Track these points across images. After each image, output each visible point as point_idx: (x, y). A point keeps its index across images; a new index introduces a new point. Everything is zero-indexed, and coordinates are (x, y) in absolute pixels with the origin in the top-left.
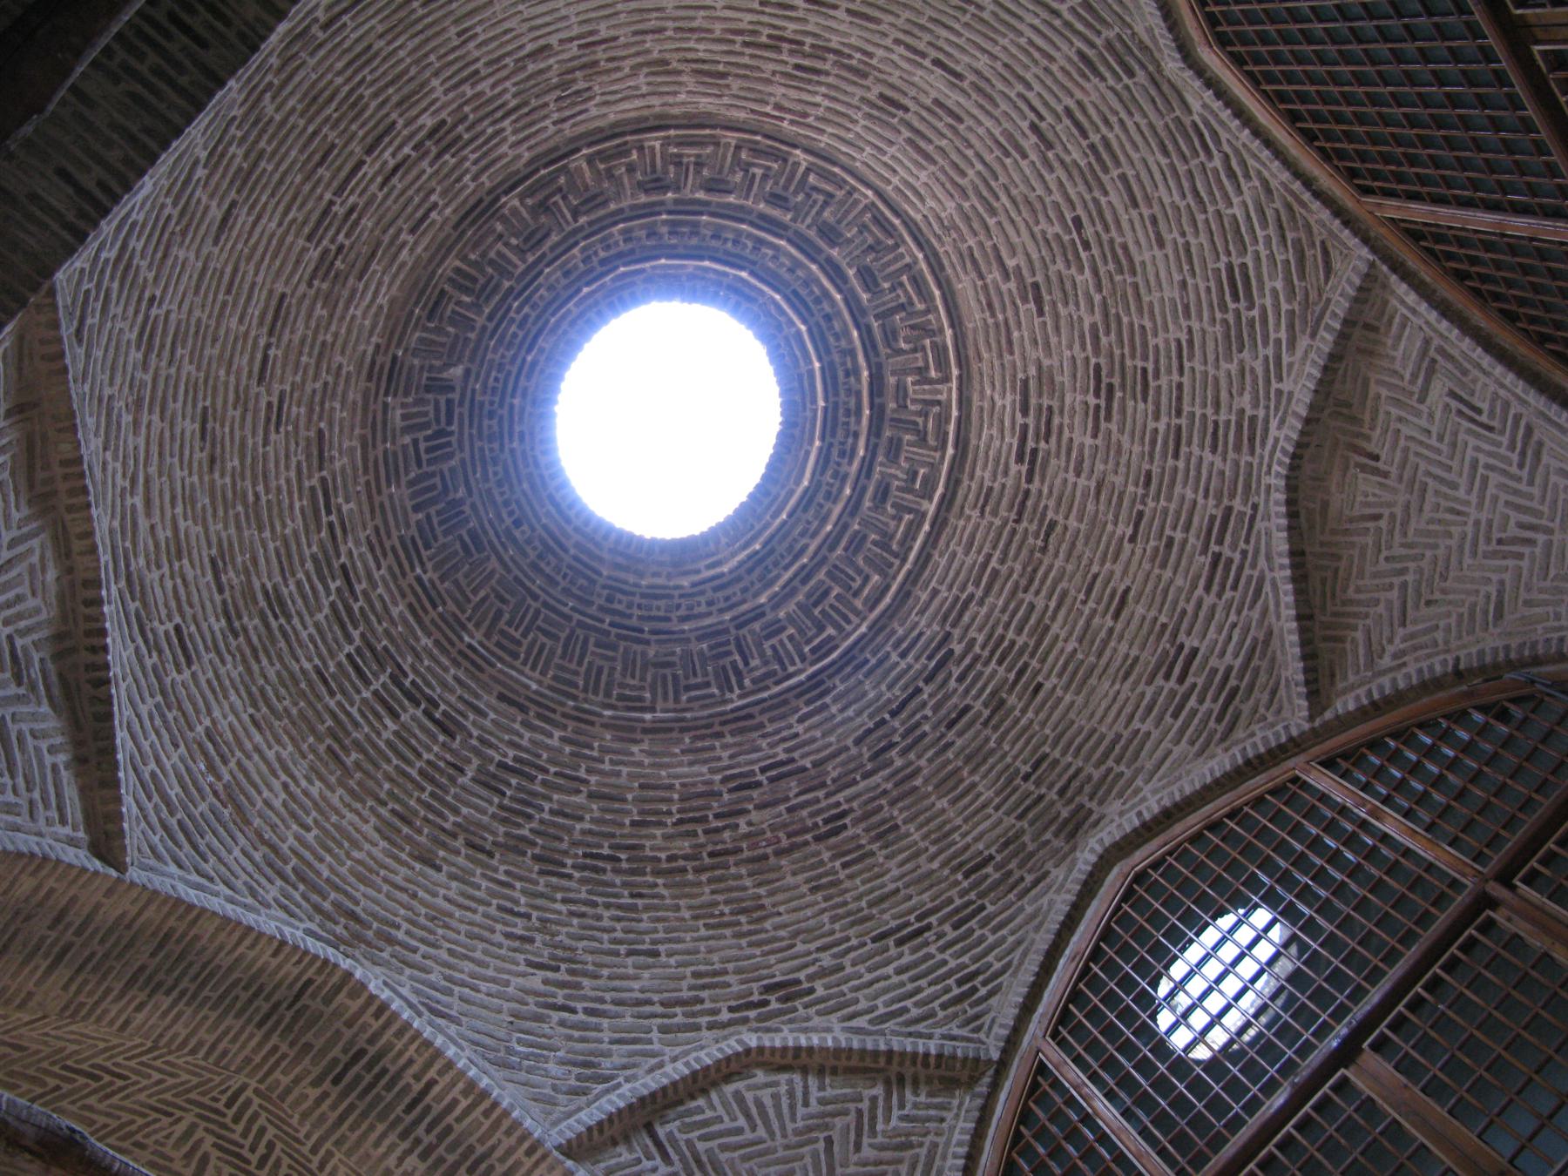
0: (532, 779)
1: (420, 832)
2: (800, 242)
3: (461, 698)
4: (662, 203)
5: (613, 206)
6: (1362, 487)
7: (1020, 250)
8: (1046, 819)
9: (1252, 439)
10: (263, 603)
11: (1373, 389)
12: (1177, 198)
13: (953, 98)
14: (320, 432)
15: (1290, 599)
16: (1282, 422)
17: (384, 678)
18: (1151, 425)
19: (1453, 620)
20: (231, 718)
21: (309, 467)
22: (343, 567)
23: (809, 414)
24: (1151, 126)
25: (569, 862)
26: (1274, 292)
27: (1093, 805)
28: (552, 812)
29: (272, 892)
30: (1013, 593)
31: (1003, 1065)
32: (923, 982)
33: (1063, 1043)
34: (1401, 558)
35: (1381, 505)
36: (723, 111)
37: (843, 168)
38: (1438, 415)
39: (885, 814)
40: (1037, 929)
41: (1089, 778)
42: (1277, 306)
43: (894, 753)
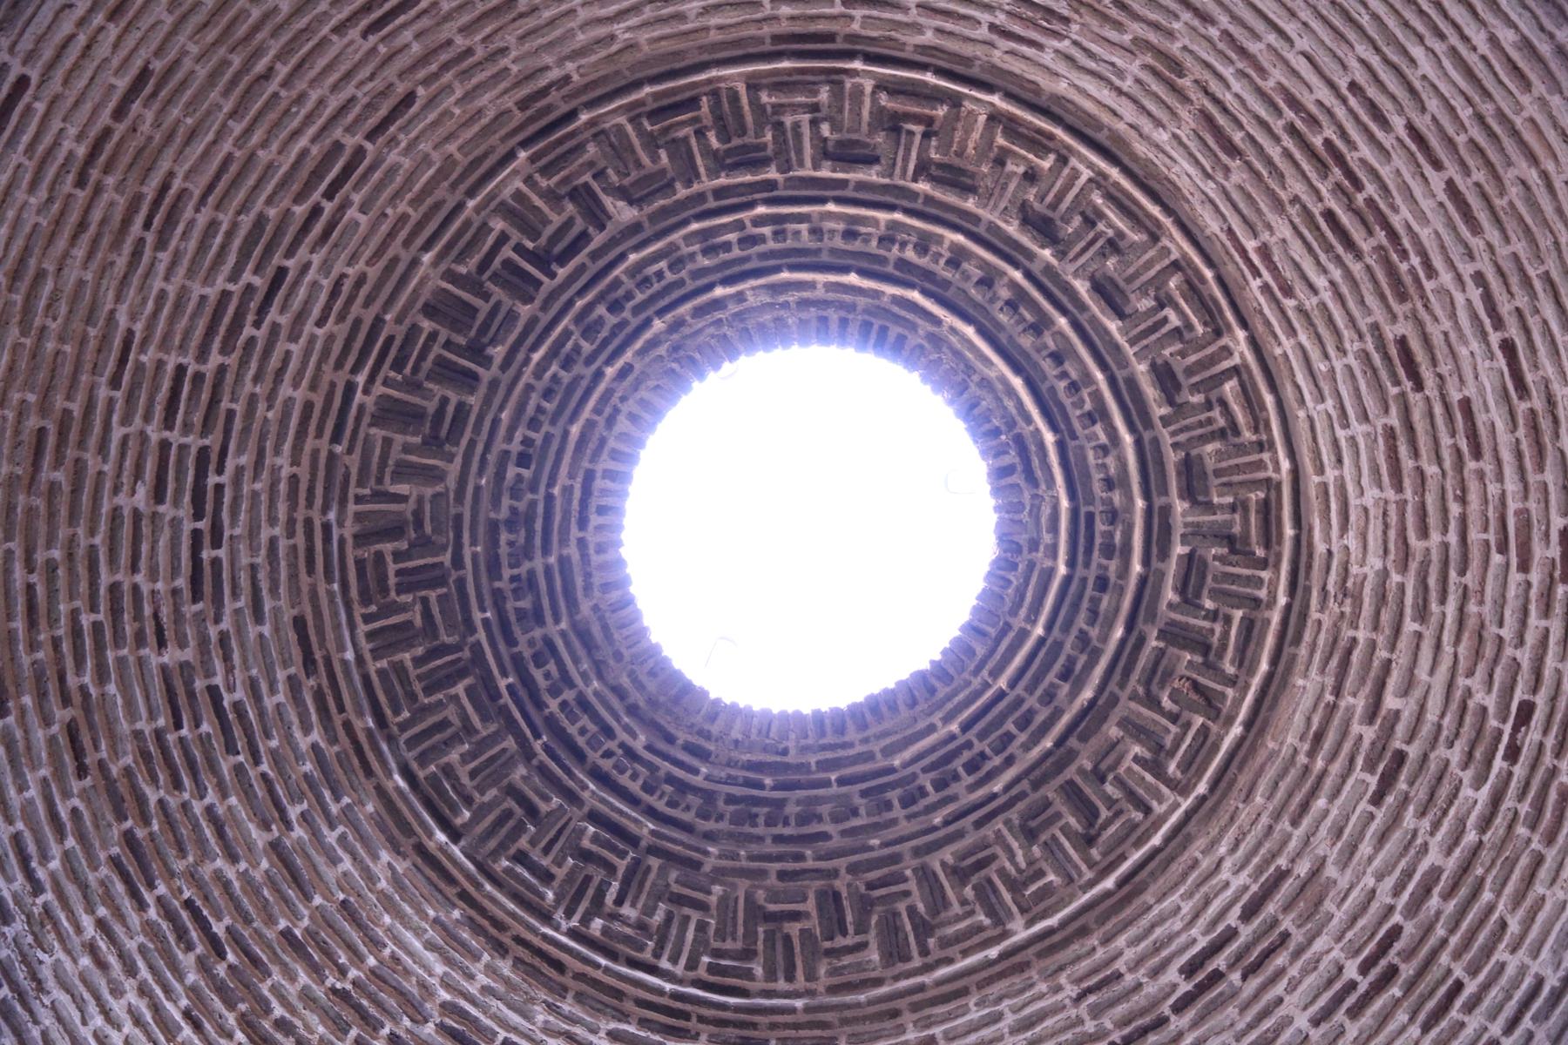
0: (231, 749)
3: (253, 568)
4: (1030, 256)
5: (970, 204)
7: (1417, 693)
10: (150, 190)
14: (409, 98)
17: (194, 441)
21: (358, 120)
22: (282, 272)
23: (976, 683)
25: (162, 889)
28: (209, 810)
36: (1196, 201)
37: (1280, 404)
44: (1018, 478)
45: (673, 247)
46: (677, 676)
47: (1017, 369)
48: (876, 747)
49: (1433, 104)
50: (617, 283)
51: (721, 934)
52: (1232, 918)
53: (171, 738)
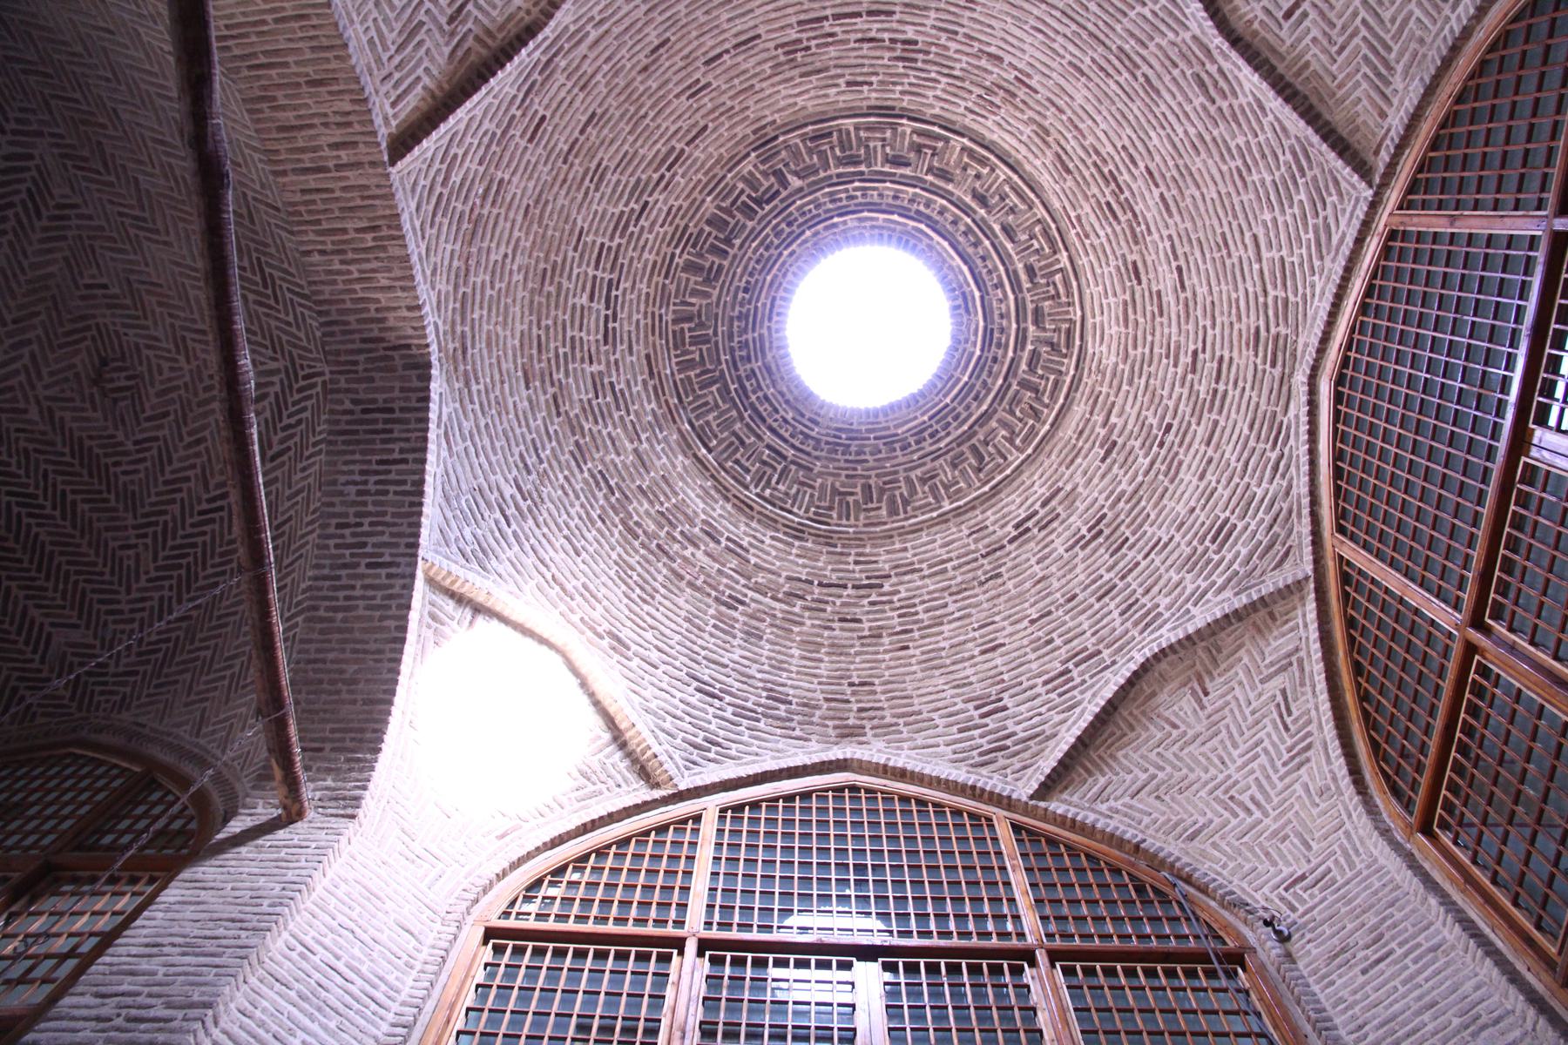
0: (618, 409)
1: (540, 361)
2: (1020, 306)
4: (975, 212)
5: (950, 187)
6: (1183, 703)
7: (1125, 416)
8: (839, 714)
9: (1148, 625)
10: (593, 166)
11: (1242, 652)
12: (1233, 459)
13: (1168, 298)
14: (705, 128)
15: (1085, 725)
16: (1174, 628)
18: (1102, 571)
19: (1162, 819)
20: (519, 192)
22: (647, 203)
24: (1258, 404)
26: (1238, 553)
27: (870, 733)
28: (609, 434)
29: (442, 286)
30: (943, 590)
31: (680, 796)
32: (688, 719)
33: (722, 818)
34: (1171, 764)
35: (1184, 722)
37: (1079, 286)
38: (1264, 698)
39: (762, 626)
40: (774, 758)
41: (883, 718)
42: (1231, 563)
43: (800, 603)
44: (962, 311)
45: (817, 199)
46: (806, 389)
47: (966, 262)
48: (891, 424)
49: (1157, 158)
50: (791, 214)
51: (819, 499)
52: (1037, 506)
53: (594, 402)
